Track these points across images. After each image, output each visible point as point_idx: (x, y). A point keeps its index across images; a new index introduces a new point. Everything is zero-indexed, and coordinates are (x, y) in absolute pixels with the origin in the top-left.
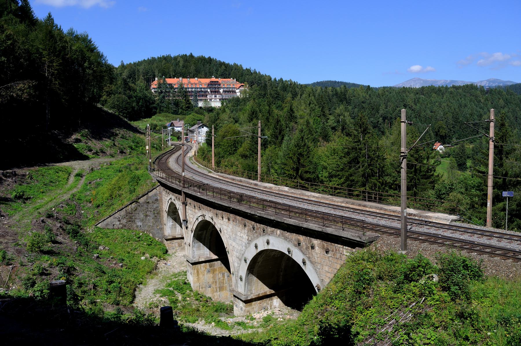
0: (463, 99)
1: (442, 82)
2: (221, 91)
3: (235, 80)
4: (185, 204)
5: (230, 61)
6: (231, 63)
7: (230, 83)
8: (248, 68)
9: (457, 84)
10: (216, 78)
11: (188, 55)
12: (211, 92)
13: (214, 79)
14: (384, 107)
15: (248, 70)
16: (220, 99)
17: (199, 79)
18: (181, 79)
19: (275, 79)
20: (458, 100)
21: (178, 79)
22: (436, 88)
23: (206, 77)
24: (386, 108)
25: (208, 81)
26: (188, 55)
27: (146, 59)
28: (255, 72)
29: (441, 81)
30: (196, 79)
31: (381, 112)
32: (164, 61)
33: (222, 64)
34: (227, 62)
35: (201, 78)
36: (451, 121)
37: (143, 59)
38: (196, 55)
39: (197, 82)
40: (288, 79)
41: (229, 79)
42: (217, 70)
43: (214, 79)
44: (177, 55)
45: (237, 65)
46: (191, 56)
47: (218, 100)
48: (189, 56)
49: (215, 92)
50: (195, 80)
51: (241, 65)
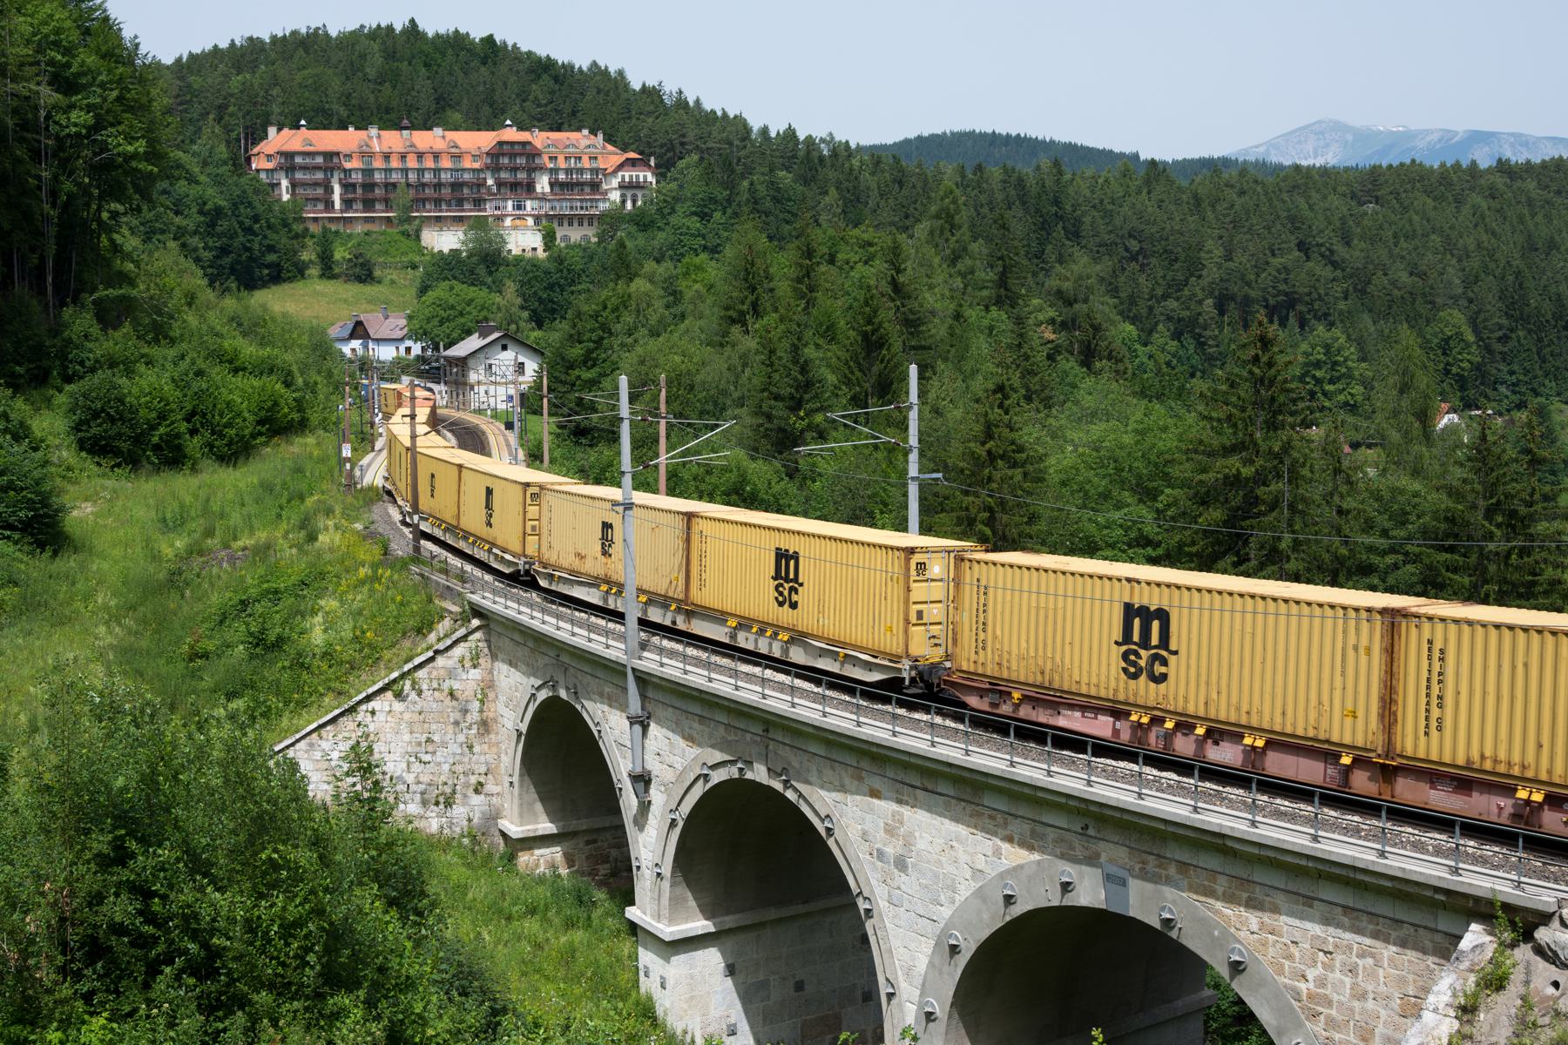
0: (1539, 218)
1: (1435, 137)
2: (543, 184)
3: (600, 136)
4: (641, 723)
5: (572, 48)
6: (582, 62)
7: (579, 146)
8: (651, 83)
9: (1518, 157)
10: (521, 128)
11: (398, 28)
12: (500, 184)
13: (511, 134)
14: (1219, 252)
15: (651, 94)
16: (537, 219)
17: (450, 135)
18: (373, 131)
19: (765, 131)
20: (1521, 219)
21: (362, 134)
22: (1431, 170)
23: (477, 124)
24: (1228, 258)
25: (484, 140)
26: (398, 28)
27: (224, 45)
28: (681, 103)
29: (1428, 132)
30: (438, 131)
31: (1211, 273)
32: (301, 51)
33: (544, 68)
34: (561, 57)
35: (456, 129)
36: (1497, 318)
37: (209, 47)
38: (433, 25)
39: (440, 145)
40: (819, 133)
41: (574, 135)
42: (523, 97)
43: (511, 134)
44: (352, 26)
45: (606, 72)
46: (412, 29)
47: (530, 221)
48: (405, 31)
49: (514, 186)
50: (432, 139)
51: (621, 73)
